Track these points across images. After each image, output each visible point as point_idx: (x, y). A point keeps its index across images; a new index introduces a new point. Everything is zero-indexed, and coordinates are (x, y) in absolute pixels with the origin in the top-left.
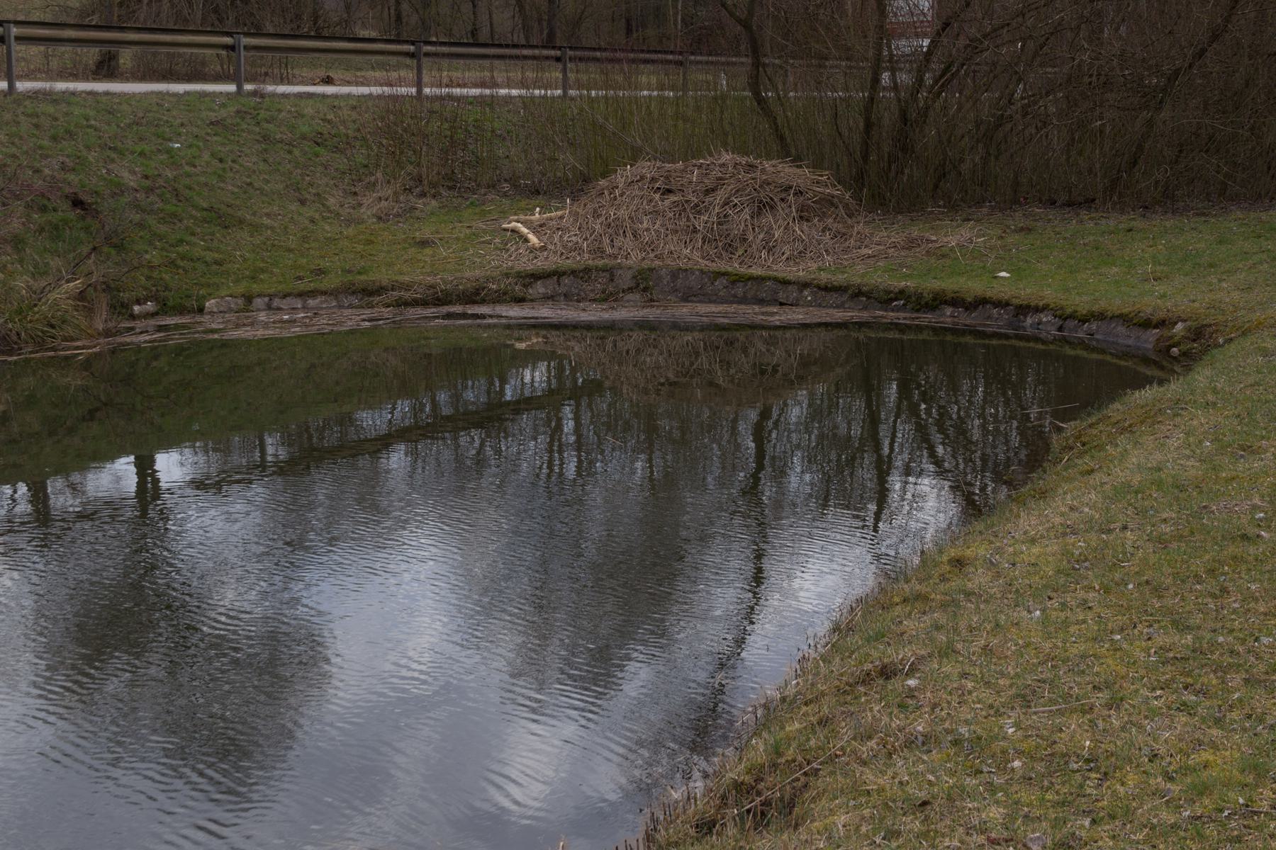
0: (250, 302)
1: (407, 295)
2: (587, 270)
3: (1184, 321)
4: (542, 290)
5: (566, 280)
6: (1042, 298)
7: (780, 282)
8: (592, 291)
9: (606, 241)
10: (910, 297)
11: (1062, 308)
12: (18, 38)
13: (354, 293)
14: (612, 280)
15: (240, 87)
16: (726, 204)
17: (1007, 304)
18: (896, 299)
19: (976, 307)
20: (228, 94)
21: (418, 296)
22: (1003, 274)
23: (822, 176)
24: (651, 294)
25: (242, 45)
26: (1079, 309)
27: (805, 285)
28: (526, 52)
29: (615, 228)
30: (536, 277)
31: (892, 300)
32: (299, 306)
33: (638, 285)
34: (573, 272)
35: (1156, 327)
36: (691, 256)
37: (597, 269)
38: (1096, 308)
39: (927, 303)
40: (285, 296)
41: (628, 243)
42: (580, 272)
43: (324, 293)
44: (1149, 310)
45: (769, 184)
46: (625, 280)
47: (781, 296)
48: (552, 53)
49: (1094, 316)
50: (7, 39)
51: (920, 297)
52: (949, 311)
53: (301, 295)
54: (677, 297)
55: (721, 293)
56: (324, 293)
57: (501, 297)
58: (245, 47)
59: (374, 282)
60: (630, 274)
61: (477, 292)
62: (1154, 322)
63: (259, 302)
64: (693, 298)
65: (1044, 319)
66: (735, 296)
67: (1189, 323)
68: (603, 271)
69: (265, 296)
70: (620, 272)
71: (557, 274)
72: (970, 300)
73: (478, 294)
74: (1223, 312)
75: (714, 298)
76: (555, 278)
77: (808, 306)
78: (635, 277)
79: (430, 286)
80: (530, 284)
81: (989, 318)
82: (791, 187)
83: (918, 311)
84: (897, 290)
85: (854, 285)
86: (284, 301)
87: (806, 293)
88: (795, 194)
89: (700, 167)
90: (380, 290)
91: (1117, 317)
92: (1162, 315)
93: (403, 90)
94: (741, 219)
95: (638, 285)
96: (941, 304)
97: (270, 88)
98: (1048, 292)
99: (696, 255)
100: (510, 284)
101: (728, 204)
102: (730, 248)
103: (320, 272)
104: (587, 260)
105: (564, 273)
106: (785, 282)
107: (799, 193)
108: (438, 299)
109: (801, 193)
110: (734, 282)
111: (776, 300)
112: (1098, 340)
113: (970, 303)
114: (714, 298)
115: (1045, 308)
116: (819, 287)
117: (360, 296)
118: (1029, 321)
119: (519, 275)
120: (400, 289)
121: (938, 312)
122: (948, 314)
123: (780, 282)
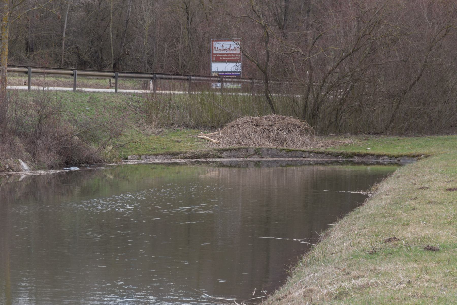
0: (140, 157)
1: (187, 155)
2: (239, 149)
3: (423, 155)
4: (226, 155)
5: (233, 152)
6: (384, 153)
7: (303, 151)
8: (242, 155)
9: (241, 140)
10: (344, 154)
11: (390, 155)
12: (33, 72)
13: (170, 155)
14: (248, 152)
15: (75, 89)
16: (278, 129)
17: (374, 155)
18: (340, 155)
19: (365, 156)
20: (111, 92)
21: (190, 155)
22: (369, 149)
23: (304, 122)
24: (261, 156)
25: (76, 74)
26: (395, 154)
27: (311, 152)
28: (143, 75)
29: (243, 136)
30: (224, 150)
31: (339, 155)
32: (155, 158)
33: (256, 153)
34: (235, 149)
35: (416, 157)
36: (269, 144)
37: (242, 148)
38: (399, 154)
39: (350, 156)
40: (150, 155)
41: (248, 141)
42: (237, 149)
43: (161, 154)
44: (414, 153)
45: (290, 124)
46: (252, 152)
47: (304, 155)
48: (186, 77)
49: (399, 156)
50: (29, 72)
51: (348, 154)
52: (357, 158)
53: (154, 155)
54: (269, 156)
55: (284, 155)
56: (161, 154)
57: (214, 156)
58: (32, 72)
59: (175, 151)
60: (253, 150)
61: (207, 155)
62: (416, 156)
63: (143, 157)
64: (275, 157)
65: (385, 158)
66: (289, 156)
67: (425, 155)
68: (244, 149)
69: (144, 155)
70: (249, 149)
71: (230, 150)
72: (363, 154)
73: (207, 155)
74: (432, 153)
75: (282, 156)
76: (229, 151)
77: (312, 158)
78: (255, 151)
79: (193, 153)
80: (222, 152)
81: (369, 159)
82: (296, 125)
83: (347, 158)
84: (340, 153)
85: (326, 152)
86: (150, 157)
87: (311, 154)
88: (297, 127)
89: (266, 118)
90: (177, 154)
91: (406, 155)
92: (418, 154)
93: (21, 87)
94: (284, 134)
95: (256, 153)
96: (354, 156)
97: (83, 89)
98: (384, 152)
99: (271, 145)
100: (216, 152)
101: (278, 129)
102: (282, 143)
103: (154, 149)
104: (235, 146)
105: (232, 149)
106: (304, 152)
107: (299, 127)
108: (196, 157)
109: (299, 127)
110: (288, 152)
111: (302, 157)
112: (401, 162)
113: (363, 155)
114: (282, 156)
115: (385, 155)
116: (315, 153)
117: (172, 156)
118: (381, 159)
119: (218, 150)
120: (183, 153)
121: (353, 158)
122: (357, 158)
123: (303, 151)
